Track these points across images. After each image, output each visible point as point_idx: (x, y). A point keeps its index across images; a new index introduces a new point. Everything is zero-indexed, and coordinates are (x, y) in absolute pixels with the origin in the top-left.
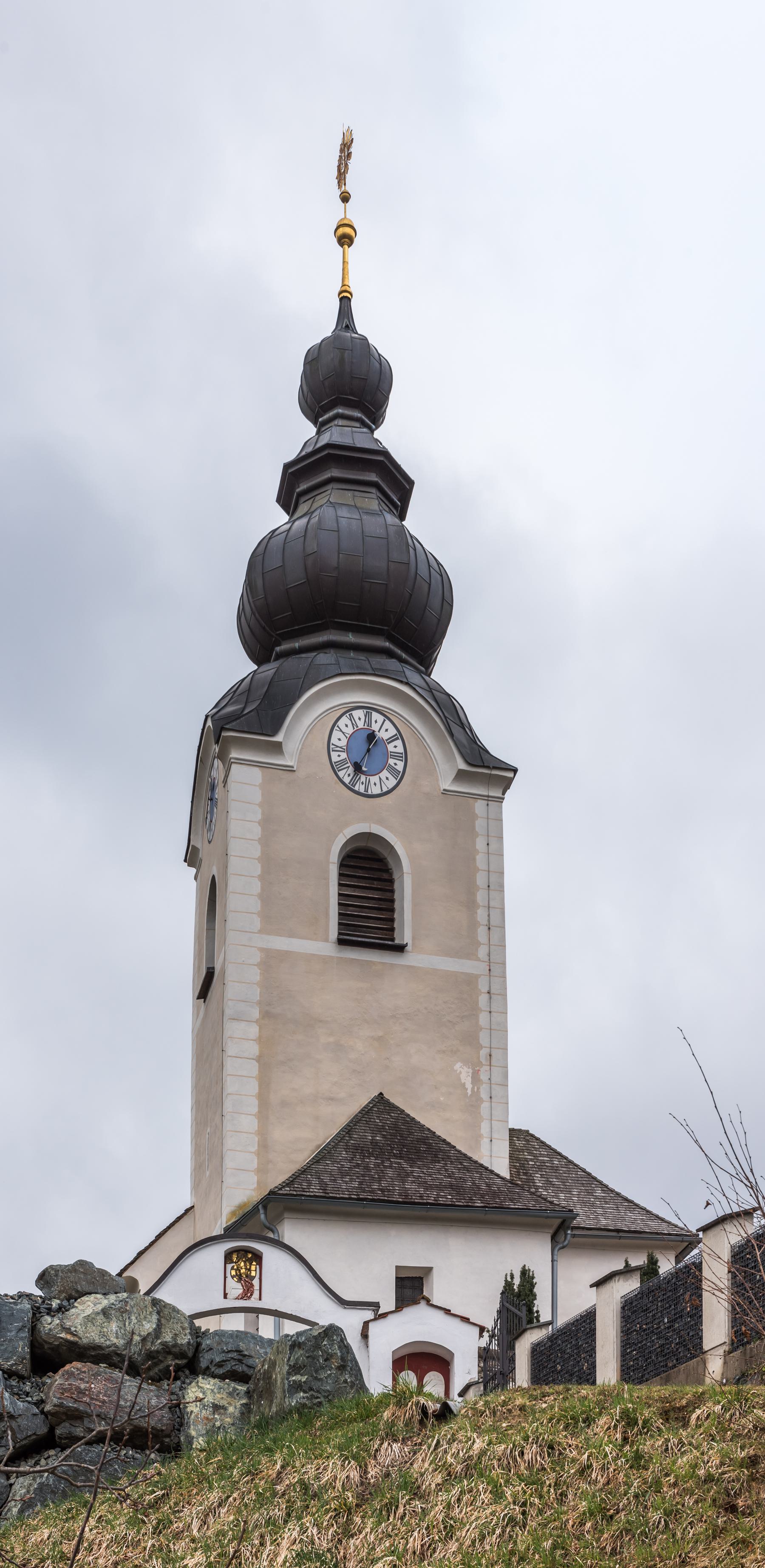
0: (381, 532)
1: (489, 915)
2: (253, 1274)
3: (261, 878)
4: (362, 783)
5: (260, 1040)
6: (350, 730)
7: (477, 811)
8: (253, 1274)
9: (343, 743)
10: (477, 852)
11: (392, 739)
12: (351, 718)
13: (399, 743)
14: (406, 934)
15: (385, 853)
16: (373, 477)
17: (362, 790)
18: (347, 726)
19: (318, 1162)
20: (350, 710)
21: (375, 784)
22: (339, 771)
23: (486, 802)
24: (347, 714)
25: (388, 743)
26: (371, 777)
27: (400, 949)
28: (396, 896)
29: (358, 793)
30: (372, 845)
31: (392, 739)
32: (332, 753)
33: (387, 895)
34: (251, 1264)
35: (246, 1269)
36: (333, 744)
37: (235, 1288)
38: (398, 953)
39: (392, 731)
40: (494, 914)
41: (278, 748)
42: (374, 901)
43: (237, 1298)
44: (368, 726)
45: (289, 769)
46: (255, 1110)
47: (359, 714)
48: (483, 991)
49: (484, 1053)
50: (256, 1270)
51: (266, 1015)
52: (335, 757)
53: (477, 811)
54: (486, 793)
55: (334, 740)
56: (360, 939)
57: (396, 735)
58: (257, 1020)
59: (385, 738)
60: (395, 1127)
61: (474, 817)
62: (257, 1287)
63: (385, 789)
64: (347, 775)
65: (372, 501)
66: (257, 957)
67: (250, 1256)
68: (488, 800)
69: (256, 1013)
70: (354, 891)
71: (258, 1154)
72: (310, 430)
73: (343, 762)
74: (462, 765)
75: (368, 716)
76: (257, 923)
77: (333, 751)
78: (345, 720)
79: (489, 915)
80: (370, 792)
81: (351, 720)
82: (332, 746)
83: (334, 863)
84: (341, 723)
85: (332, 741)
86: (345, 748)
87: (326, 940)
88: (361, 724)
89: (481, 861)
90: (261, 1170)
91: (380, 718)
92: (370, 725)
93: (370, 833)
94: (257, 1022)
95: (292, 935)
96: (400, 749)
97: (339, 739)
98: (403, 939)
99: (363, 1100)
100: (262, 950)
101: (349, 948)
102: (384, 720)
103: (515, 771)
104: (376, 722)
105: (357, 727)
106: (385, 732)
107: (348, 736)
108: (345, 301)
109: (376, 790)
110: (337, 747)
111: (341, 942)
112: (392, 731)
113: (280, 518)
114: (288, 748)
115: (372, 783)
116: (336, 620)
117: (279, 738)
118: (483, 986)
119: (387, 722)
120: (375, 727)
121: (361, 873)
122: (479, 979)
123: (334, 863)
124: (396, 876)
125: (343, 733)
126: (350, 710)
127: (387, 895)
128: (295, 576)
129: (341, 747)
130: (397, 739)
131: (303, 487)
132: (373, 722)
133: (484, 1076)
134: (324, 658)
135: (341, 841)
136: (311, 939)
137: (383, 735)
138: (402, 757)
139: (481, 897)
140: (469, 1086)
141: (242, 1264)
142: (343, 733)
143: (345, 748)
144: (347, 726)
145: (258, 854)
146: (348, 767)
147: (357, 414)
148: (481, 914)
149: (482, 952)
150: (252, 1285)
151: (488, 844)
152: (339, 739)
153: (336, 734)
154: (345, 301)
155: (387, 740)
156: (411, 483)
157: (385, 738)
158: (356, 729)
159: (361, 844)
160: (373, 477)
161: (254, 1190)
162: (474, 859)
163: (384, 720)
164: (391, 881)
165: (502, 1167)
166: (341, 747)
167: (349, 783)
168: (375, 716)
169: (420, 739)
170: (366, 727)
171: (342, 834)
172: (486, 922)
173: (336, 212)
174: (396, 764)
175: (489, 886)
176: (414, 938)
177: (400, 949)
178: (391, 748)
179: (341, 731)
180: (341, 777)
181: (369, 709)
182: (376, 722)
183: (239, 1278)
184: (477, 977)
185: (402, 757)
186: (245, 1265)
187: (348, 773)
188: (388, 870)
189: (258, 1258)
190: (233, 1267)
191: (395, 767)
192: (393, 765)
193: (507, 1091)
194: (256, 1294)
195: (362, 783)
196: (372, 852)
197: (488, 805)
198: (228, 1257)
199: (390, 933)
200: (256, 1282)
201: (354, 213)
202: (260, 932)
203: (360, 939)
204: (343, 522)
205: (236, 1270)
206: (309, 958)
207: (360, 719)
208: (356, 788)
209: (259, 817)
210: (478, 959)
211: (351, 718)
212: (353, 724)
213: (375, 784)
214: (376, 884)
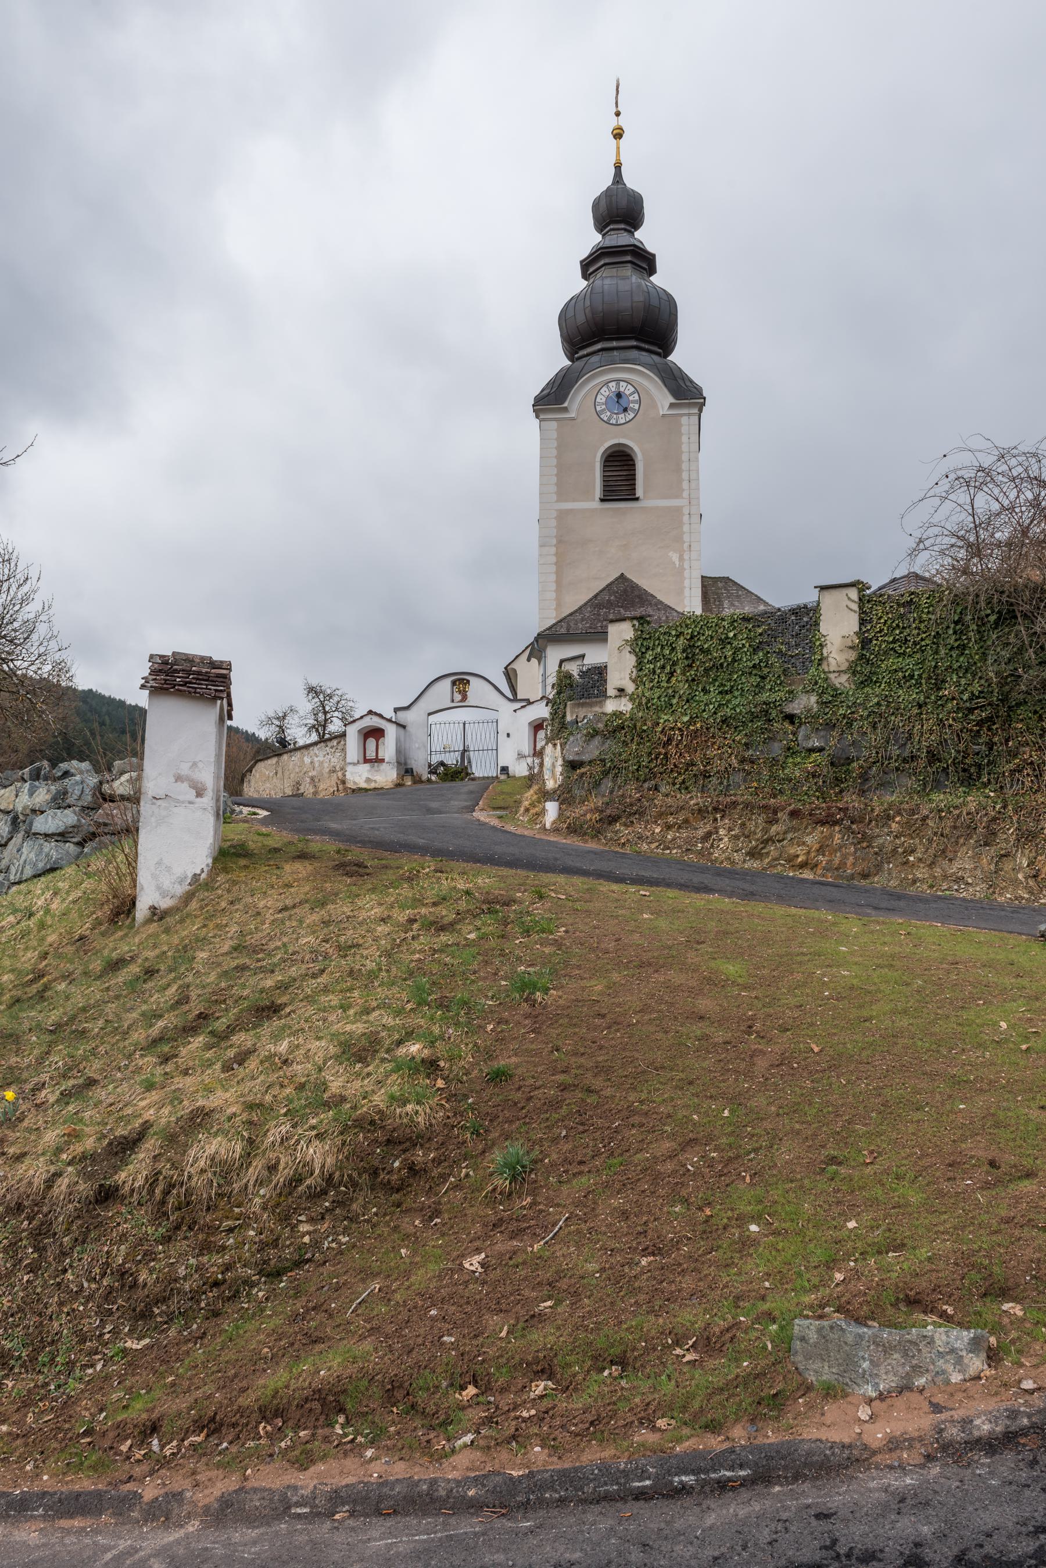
0: (627, 288)
3: (557, 475)
5: (557, 554)
9: (604, 400)
14: (639, 492)
15: (629, 452)
16: (629, 258)
20: (607, 383)
27: (637, 499)
30: (622, 449)
37: (458, 697)
41: (566, 410)
45: (573, 419)
46: (554, 588)
49: (686, 545)
51: (560, 542)
55: (598, 400)
60: (625, 591)
61: (681, 425)
65: (628, 271)
66: (555, 514)
69: (554, 541)
71: (556, 609)
72: (597, 238)
74: (673, 401)
75: (618, 385)
76: (554, 497)
78: (604, 388)
84: (602, 391)
91: (625, 384)
95: (574, 501)
97: (601, 399)
99: (617, 575)
108: (618, 167)
111: (602, 500)
113: (585, 283)
117: (566, 405)
118: (686, 511)
120: (622, 389)
126: (607, 383)
128: (581, 319)
131: (591, 270)
133: (686, 557)
134: (595, 359)
135: (602, 450)
140: (677, 563)
147: (622, 226)
148: (685, 475)
149: (685, 494)
153: (599, 396)
154: (618, 167)
156: (654, 256)
159: (617, 449)
160: (629, 258)
165: (692, 604)
169: (648, 392)
173: (613, 122)
176: (644, 492)
177: (637, 499)
178: (631, 398)
181: (618, 381)
183: (460, 692)
189: (468, 682)
196: (623, 451)
198: (454, 683)
201: (622, 121)
202: (557, 501)
204: (606, 287)
209: (555, 445)
214: (626, 468)
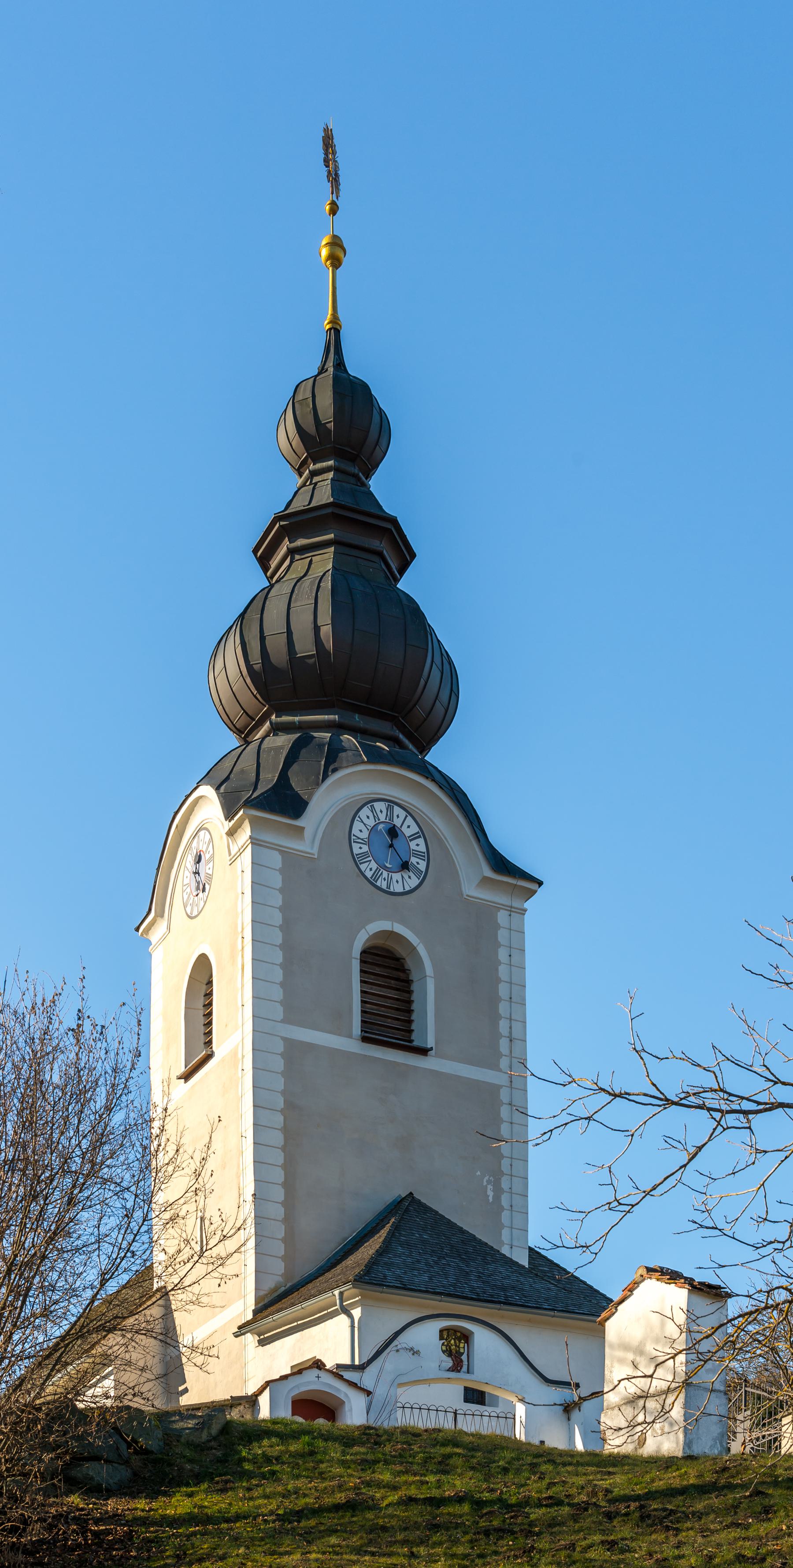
1: (511, 1028)
2: (462, 1350)
4: (385, 879)
6: (371, 822)
7: (500, 921)
8: (462, 1350)
9: (365, 835)
10: (500, 963)
11: (414, 837)
12: (373, 809)
13: (421, 841)
17: (384, 886)
18: (368, 817)
19: (381, 1255)
21: (397, 882)
22: (361, 864)
23: (509, 913)
24: (369, 805)
25: (411, 840)
26: (393, 874)
27: (423, 1051)
28: (414, 997)
29: (380, 889)
30: (390, 944)
31: (414, 837)
32: (354, 845)
33: (404, 996)
34: (460, 1342)
35: (456, 1346)
36: (354, 835)
38: (422, 1057)
39: (415, 829)
40: (516, 1026)
42: (391, 1001)
43: (448, 1370)
44: (390, 820)
47: (380, 806)
48: (505, 1101)
50: (464, 1348)
52: (356, 849)
53: (499, 921)
54: (509, 904)
55: (355, 831)
56: (377, 1037)
57: (418, 833)
58: (282, 1109)
59: (407, 835)
61: (497, 927)
62: (465, 1363)
63: (407, 888)
64: (368, 869)
67: (459, 1334)
68: (511, 911)
69: (280, 1103)
70: (371, 989)
73: (365, 854)
75: (390, 809)
77: (354, 842)
79: (511, 1028)
80: (392, 890)
81: (372, 812)
82: (353, 837)
83: (357, 959)
85: (353, 832)
86: (366, 840)
87: (350, 1036)
88: (382, 817)
89: (503, 971)
90: (287, 1258)
91: (403, 814)
92: (391, 819)
93: (392, 932)
94: (282, 1111)
96: (422, 848)
97: (360, 830)
98: (427, 1044)
100: (285, 1039)
101: (401, 1050)
102: (406, 816)
103: (540, 883)
104: (398, 816)
105: (379, 820)
106: (409, 828)
107: (370, 828)
108: (335, 330)
109: (398, 888)
110: (359, 838)
111: (365, 1039)
112: (415, 829)
114: (308, 833)
115: (394, 880)
116: (344, 699)
118: (504, 1095)
119: (409, 818)
120: (397, 822)
121: (378, 970)
122: (501, 1090)
123: (357, 959)
124: (414, 976)
125: (365, 824)
126: (370, 802)
127: (404, 996)
129: (362, 839)
130: (419, 837)
132: (395, 817)
136: (335, 1034)
137: (408, 832)
138: (424, 856)
139: (503, 1009)
141: (452, 1342)
142: (365, 824)
143: (366, 840)
144: (368, 817)
145: (279, 940)
146: (370, 861)
148: (503, 1026)
149: (504, 1063)
150: (462, 1361)
151: (510, 956)
152: (361, 831)
153: (357, 825)
155: (409, 837)
156: (413, 555)
157: (407, 835)
158: (377, 822)
161: (282, 1276)
162: (497, 970)
163: (406, 816)
164: (409, 982)
166: (362, 839)
167: (371, 878)
168: (397, 810)
170: (387, 821)
171: (364, 930)
172: (508, 1035)
174: (418, 863)
175: (511, 998)
176: (437, 1043)
178: (413, 845)
179: (362, 822)
180: (363, 870)
181: (391, 803)
182: (398, 816)
184: (499, 1087)
185: (424, 856)
186: (455, 1342)
187: (370, 867)
188: (405, 971)
190: (444, 1343)
191: (418, 866)
192: (416, 864)
193: (527, 1201)
194: (465, 1368)
195: (385, 879)
197: (510, 915)
199: (408, 1034)
200: (464, 1358)
202: (282, 1021)
203: (377, 1037)
205: (446, 1346)
206: (332, 1053)
207: (381, 812)
208: (378, 884)
210: (500, 1070)
211: (373, 809)
212: (374, 816)
213: (397, 882)
